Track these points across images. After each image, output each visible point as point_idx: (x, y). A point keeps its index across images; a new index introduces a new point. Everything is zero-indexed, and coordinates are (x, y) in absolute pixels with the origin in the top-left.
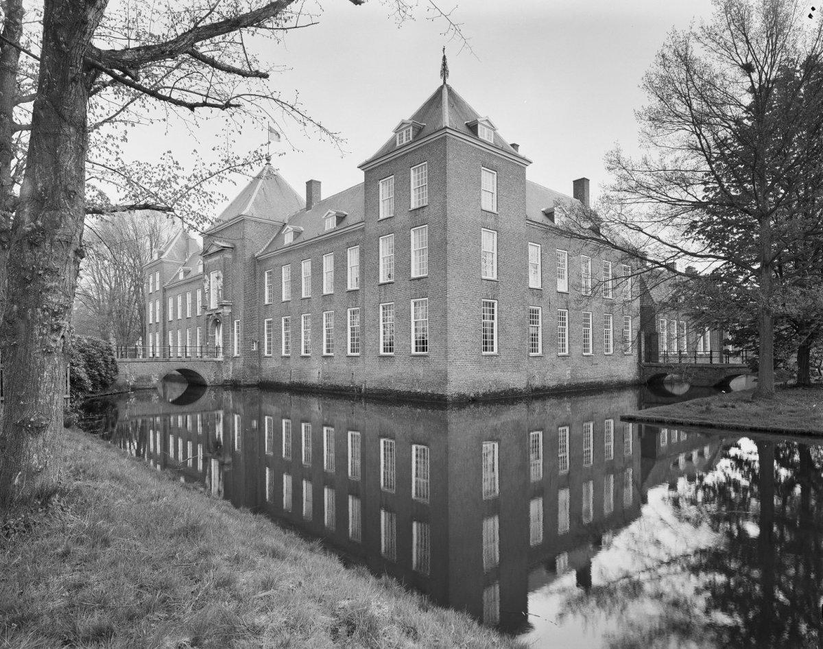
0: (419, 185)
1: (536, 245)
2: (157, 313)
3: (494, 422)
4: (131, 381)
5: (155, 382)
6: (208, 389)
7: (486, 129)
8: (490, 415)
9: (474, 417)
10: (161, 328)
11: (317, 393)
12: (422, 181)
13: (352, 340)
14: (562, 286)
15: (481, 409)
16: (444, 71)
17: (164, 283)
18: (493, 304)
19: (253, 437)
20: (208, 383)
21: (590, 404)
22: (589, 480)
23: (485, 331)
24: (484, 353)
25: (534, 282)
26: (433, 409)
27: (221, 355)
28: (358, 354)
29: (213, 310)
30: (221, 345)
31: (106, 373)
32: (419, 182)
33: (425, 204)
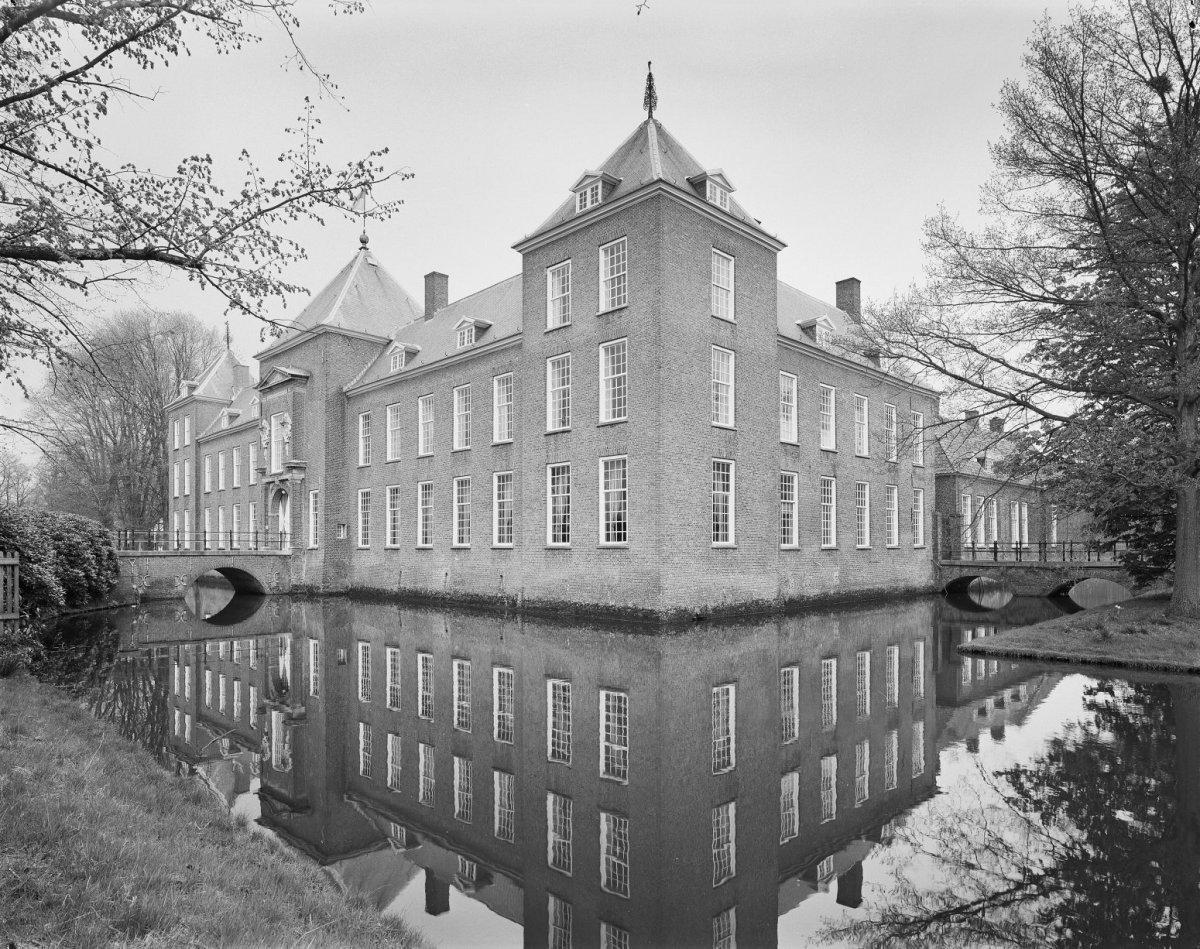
0: (612, 274)
1: (788, 374)
2: (187, 479)
3: (731, 653)
4: (139, 587)
5: (180, 588)
6: (267, 600)
7: (719, 190)
8: (724, 642)
9: (699, 647)
10: (192, 503)
11: (443, 606)
12: (618, 267)
13: (501, 522)
14: (828, 442)
15: (711, 631)
16: (650, 100)
17: (197, 434)
18: (728, 465)
19: (337, 669)
20: (267, 590)
21: (867, 623)
22: (863, 739)
23: (715, 508)
24: (715, 544)
25: (789, 433)
26: (635, 632)
27: (288, 545)
28: (510, 545)
29: (275, 475)
30: (288, 530)
31: (98, 575)
32: (612, 269)
33: (623, 305)
